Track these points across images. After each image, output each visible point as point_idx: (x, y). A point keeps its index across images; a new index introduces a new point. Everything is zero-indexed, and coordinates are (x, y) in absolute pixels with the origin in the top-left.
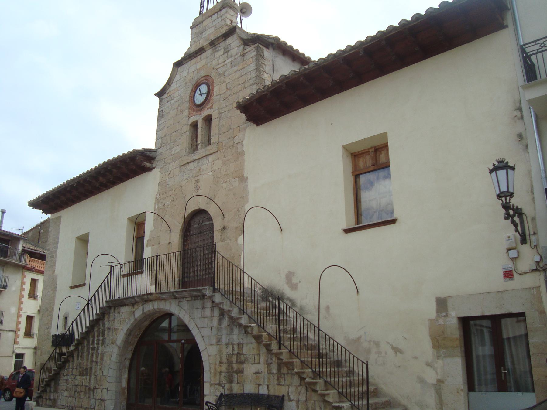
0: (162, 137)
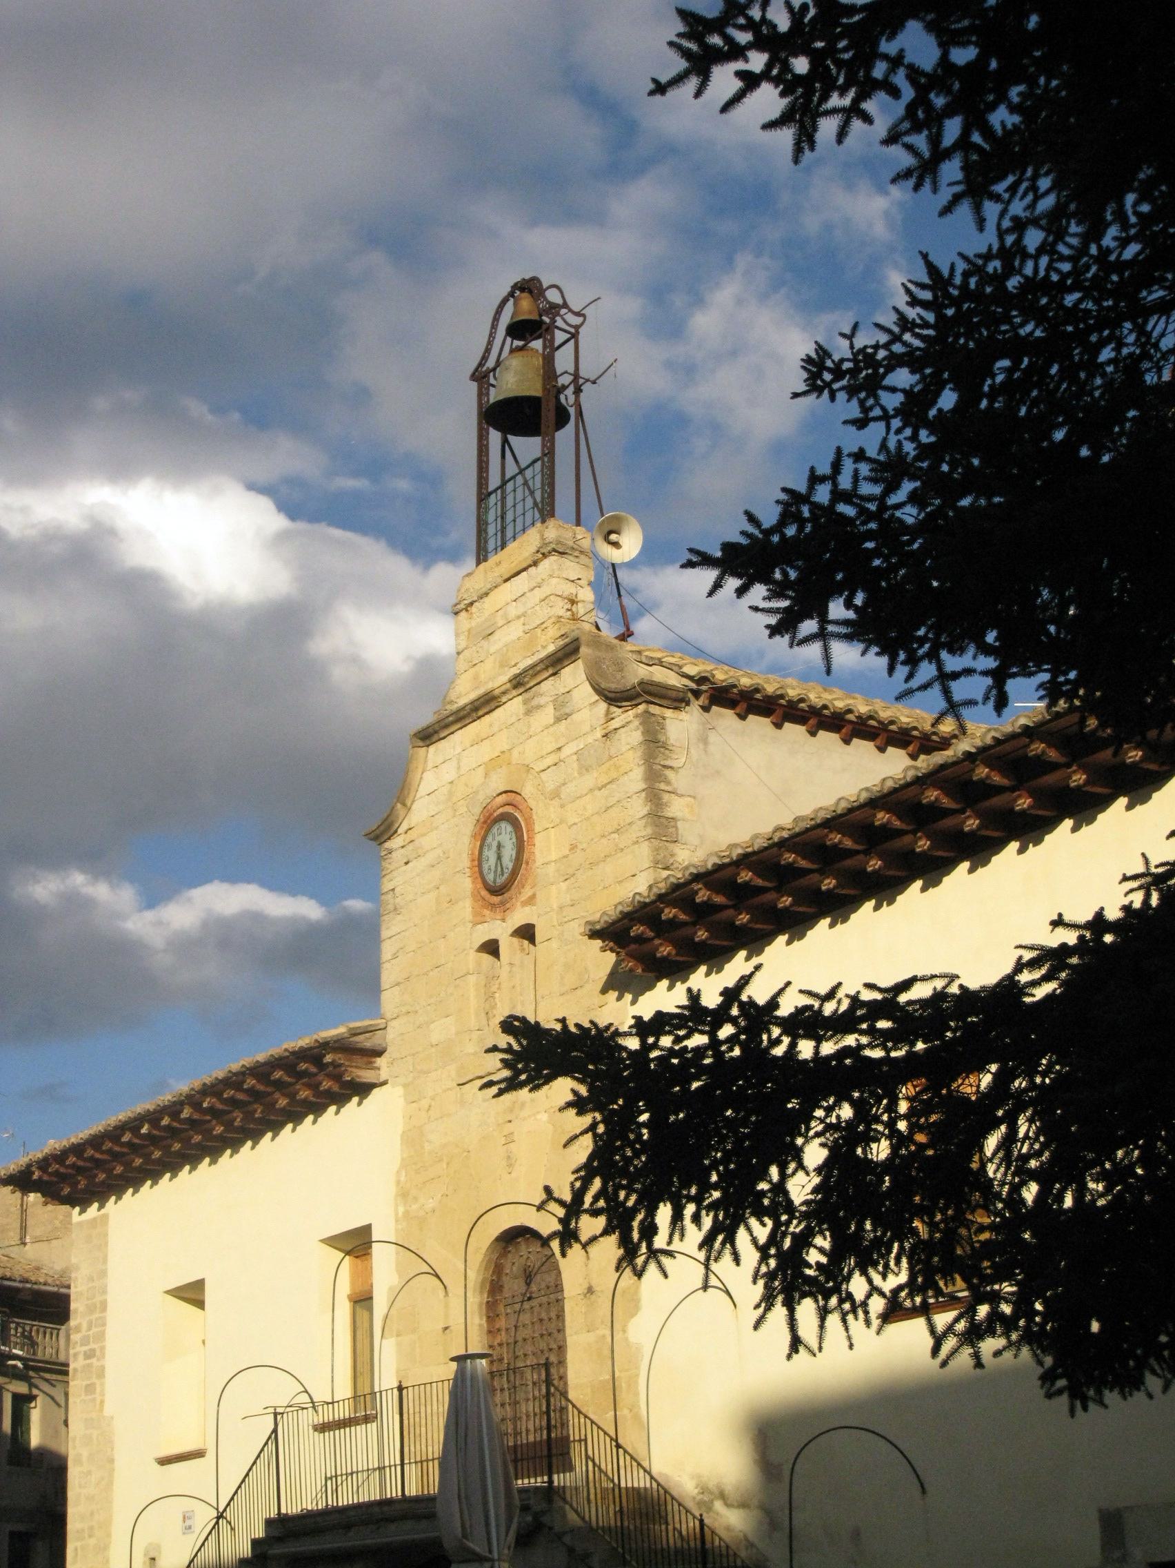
0: (400, 980)
